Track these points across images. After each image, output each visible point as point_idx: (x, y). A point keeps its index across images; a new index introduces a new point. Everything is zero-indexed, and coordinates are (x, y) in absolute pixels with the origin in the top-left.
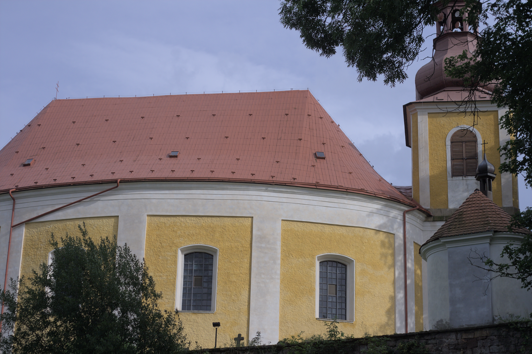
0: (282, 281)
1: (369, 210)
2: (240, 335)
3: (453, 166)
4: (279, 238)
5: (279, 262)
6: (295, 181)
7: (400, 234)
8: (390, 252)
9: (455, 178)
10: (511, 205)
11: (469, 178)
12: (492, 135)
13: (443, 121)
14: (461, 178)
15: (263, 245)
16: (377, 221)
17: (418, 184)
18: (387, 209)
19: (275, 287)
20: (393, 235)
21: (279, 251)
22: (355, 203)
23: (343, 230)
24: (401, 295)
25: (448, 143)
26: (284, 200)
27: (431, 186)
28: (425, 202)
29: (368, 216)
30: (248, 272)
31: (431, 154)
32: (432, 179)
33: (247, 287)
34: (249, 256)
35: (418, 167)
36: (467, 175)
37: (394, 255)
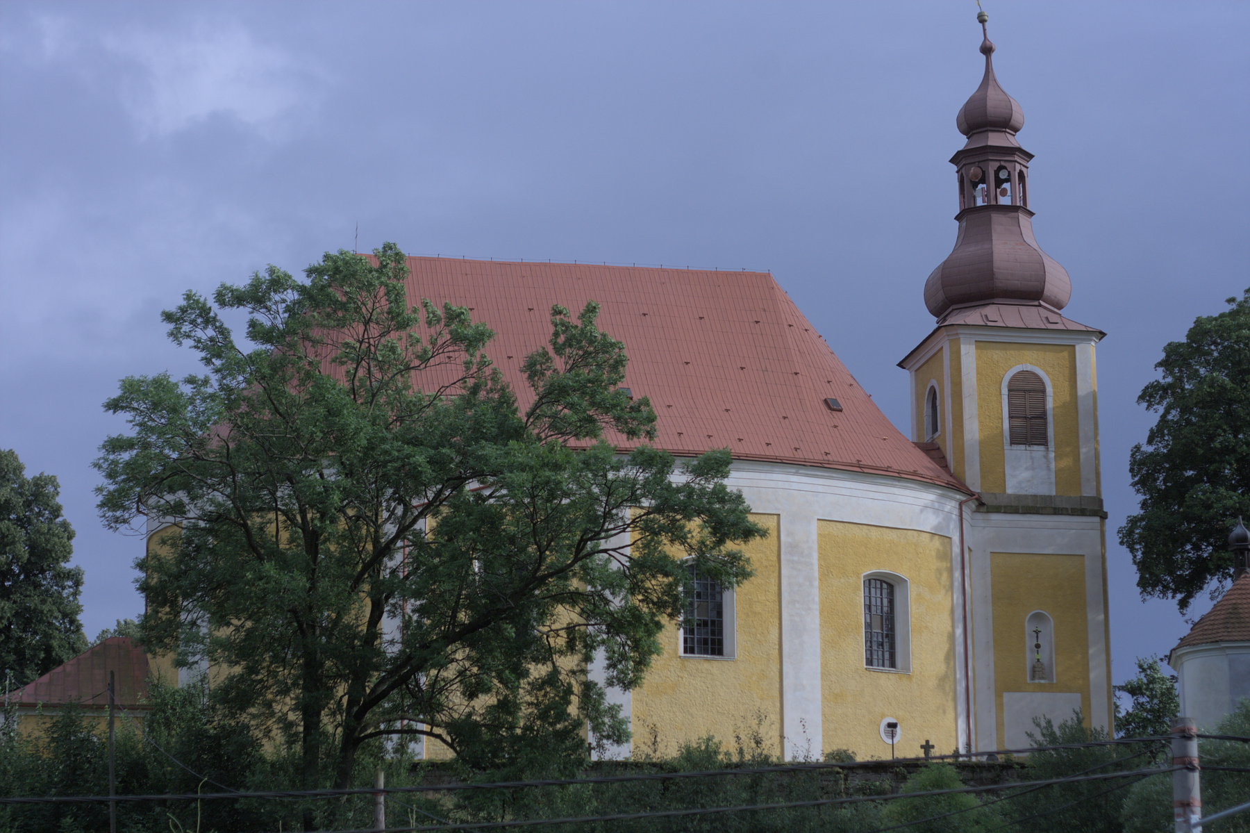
0: (821, 613)
1: (922, 502)
2: (927, 742)
3: (1011, 428)
4: (815, 547)
5: (816, 583)
6: (829, 457)
7: (956, 538)
8: (945, 564)
9: (1015, 447)
10: (1093, 493)
11: (1035, 448)
12: (1026, 353)
13: (997, 354)
14: (1023, 447)
15: (796, 558)
16: (930, 522)
17: (963, 452)
18: (943, 501)
19: (813, 621)
20: (946, 540)
21: (816, 567)
22: (907, 492)
23: (892, 535)
24: (959, 631)
25: (1005, 391)
26: (820, 489)
27: (981, 457)
28: (974, 480)
29: (922, 511)
30: (776, 598)
31: (981, 407)
32: (983, 444)
33: (777, 621)
34: (776, 574)
35: (961, 426)
36: (1031, 444)
37: (951, 571)
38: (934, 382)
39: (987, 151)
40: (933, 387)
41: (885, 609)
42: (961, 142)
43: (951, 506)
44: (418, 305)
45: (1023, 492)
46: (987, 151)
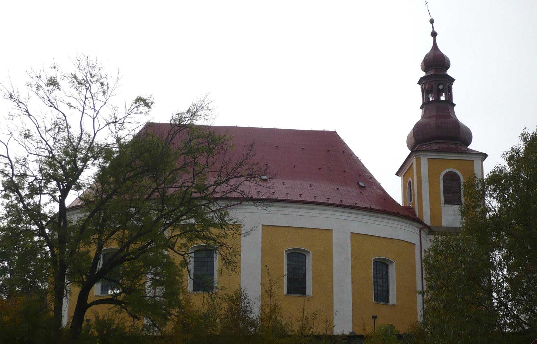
11: (456, 206)
14: (450, 205)
25: (441, 180)
26: (351, 219)
28: (427, 220)
35: (422, 203)
38: (410, 179)
39: (436, 74)
40: (410, 181)
41: (384, 288)
42: (423, 74)
43: (417, 231)
44: (56, 119)
45: (450, 226)
46: (436, 74)
